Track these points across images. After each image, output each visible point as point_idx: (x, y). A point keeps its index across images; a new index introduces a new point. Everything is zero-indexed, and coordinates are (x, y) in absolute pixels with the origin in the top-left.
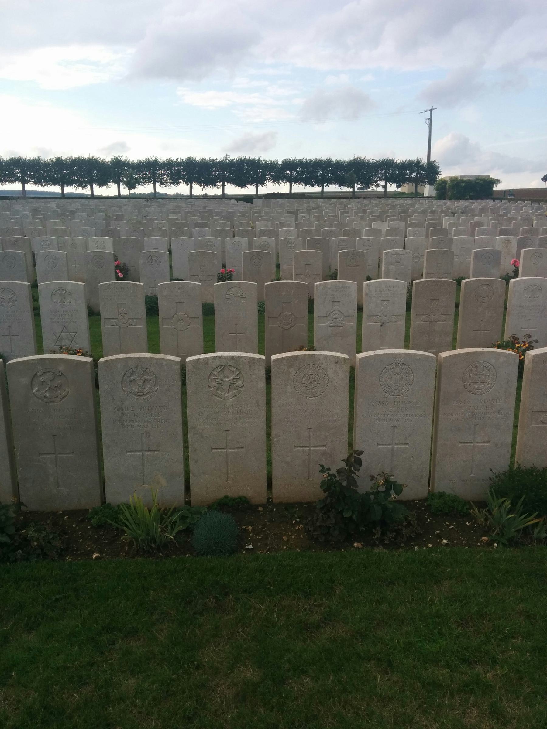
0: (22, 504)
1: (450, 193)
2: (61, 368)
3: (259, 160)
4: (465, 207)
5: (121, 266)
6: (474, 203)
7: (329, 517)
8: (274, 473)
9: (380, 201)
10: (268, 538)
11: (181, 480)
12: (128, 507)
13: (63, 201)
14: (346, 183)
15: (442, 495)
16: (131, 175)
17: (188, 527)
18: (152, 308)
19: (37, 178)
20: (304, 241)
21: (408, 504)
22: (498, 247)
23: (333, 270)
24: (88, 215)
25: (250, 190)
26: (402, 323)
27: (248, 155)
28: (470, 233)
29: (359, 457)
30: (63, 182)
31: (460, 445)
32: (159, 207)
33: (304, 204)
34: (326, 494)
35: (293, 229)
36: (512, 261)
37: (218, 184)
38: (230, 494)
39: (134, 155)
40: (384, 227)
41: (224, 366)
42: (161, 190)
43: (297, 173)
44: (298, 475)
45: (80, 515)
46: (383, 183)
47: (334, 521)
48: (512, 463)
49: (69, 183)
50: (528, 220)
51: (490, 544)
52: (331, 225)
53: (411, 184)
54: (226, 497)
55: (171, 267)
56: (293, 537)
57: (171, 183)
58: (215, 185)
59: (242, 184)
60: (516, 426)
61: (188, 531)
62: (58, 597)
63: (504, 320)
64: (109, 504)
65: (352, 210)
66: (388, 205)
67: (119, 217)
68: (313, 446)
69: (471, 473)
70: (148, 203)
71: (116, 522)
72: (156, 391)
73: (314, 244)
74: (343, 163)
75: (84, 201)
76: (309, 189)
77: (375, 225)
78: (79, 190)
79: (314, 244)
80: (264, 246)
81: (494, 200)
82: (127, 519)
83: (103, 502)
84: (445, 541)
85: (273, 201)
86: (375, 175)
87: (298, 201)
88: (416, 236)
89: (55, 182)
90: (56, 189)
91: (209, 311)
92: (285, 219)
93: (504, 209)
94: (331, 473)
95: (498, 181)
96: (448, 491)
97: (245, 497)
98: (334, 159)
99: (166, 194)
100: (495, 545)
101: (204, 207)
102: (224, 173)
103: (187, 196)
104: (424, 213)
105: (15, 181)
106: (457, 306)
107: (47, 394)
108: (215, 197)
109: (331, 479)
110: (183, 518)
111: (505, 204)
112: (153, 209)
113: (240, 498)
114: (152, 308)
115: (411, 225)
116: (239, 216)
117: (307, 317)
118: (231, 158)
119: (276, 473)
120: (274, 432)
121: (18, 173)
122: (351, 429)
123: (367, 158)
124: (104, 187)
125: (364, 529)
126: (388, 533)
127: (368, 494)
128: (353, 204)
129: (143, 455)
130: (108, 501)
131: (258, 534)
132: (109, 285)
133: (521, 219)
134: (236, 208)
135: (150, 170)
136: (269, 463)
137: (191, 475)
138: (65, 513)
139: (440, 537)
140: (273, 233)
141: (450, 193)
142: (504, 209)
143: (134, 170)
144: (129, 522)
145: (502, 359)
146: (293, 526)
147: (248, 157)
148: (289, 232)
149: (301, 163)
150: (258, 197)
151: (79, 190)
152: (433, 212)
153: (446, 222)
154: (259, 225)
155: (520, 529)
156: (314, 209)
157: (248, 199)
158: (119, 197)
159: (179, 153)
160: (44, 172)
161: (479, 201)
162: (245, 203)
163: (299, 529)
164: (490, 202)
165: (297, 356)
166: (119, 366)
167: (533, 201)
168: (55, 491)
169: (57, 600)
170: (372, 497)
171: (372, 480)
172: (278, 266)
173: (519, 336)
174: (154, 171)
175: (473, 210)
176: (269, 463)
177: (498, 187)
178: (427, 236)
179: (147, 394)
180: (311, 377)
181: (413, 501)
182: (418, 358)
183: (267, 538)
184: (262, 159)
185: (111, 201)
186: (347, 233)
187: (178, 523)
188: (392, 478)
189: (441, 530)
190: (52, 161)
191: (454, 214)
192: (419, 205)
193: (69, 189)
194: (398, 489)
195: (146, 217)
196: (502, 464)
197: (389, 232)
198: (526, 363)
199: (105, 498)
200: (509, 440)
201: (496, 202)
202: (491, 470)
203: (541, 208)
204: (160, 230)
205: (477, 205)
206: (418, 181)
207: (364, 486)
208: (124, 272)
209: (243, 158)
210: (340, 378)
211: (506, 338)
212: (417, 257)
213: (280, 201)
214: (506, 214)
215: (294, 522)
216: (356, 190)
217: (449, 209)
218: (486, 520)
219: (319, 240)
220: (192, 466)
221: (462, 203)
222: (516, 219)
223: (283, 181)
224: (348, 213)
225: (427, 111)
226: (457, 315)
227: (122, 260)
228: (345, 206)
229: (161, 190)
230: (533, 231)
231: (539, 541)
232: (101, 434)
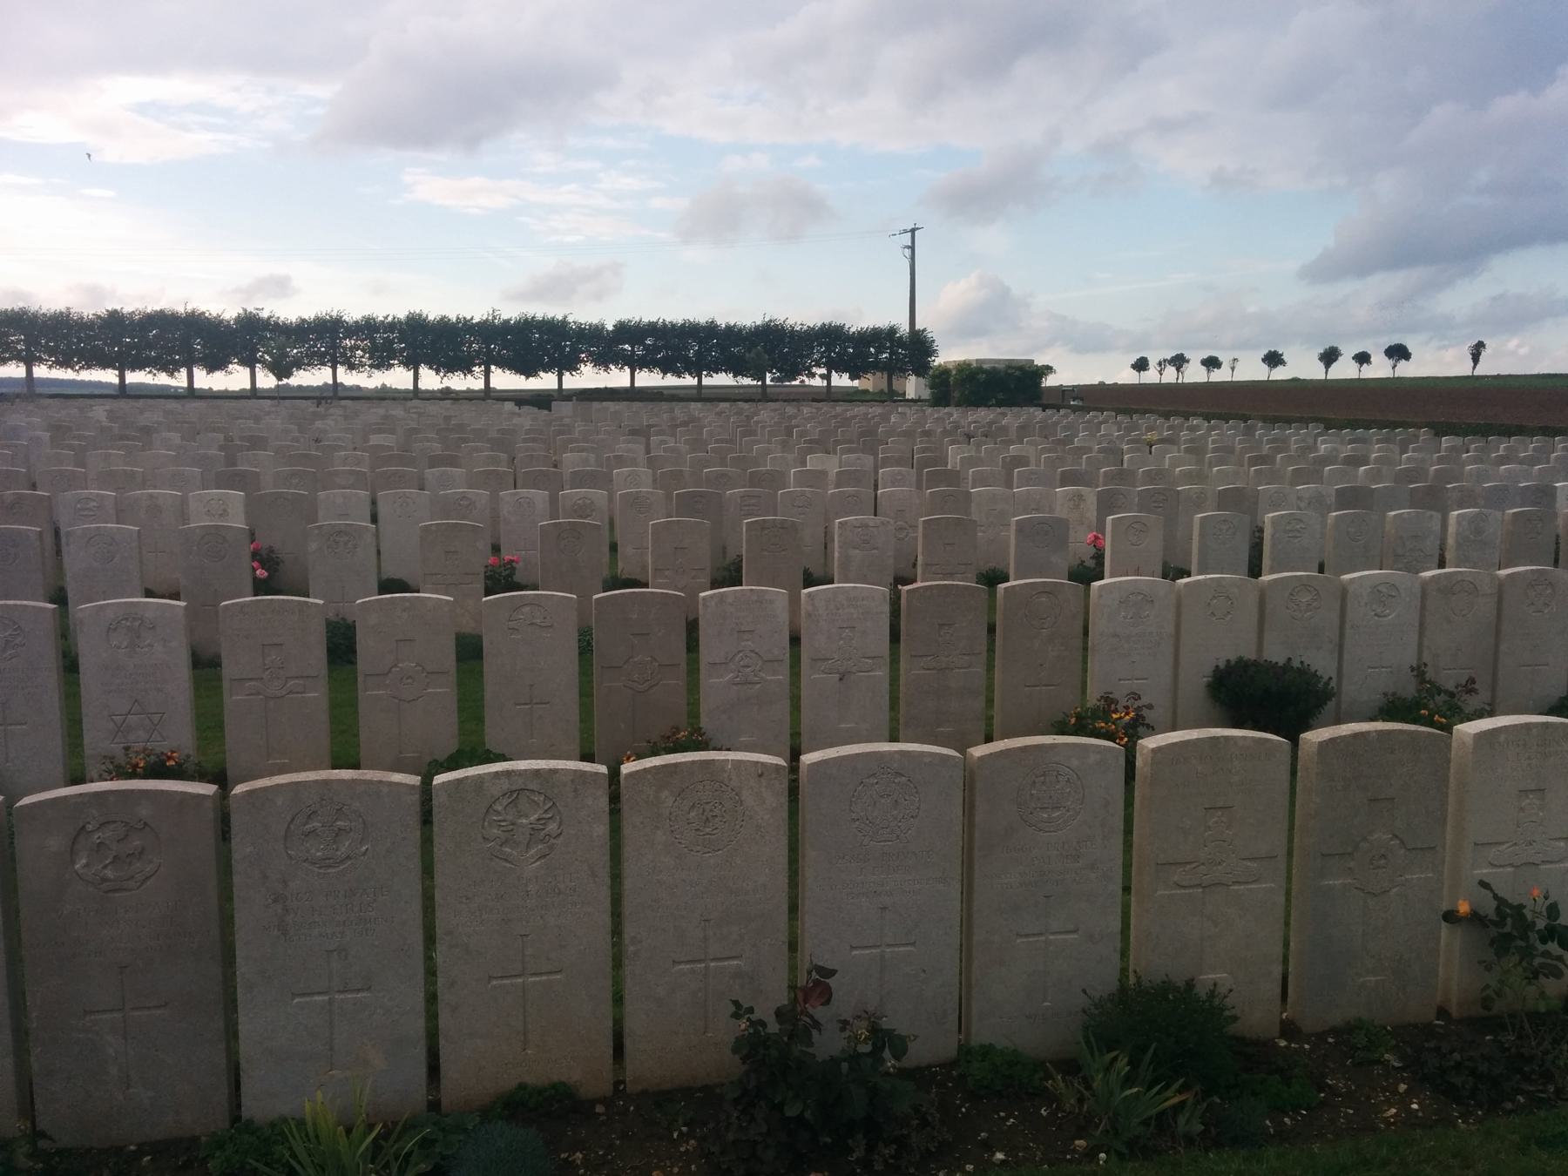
0: (43, 1135)
1: (956, 394)
2: (144, 811)
3: (564, 322)
4: (990, 424)
5: (264, 553)
6: (1005, 415)
9: (819, 409)
11: (420, 1052)
12: (301, 1123)
13: (123, 404)
14: (748, 370)
15: (986, 1051)
16: (282, 348)
18: (341, 645)
19: (63, 353)
20: (669, 497)
21: (920, 1076)
22: (1061, 512)
23: (731, 556)
24: (183, 438)
25: (546, 381)
26: (882, 673)
27: (541, 310)
28: (1010, 487)
30: (123, 363)
32: (346, 417)
33: (663, 412)
34: (745, 1068)
35: (644, 471)
36: (1090, 536)
37: (476, 369)
38: (530, 1080)
39: (289, 310)
40: (832, 465)
41: (519, 790)
42: (347, 378)
43: (646, 348)
44: (682, 1027)
46: (823, 371)
48: (1124, 971)
49: (138, 365)
50: (1114, 454)
51: (1090, 1154)
52: (723, 463)
53: (879, 374)
55: (379, 552)
57: (371, 366)
58: (471, 372)
59: (528, 371)
60: (1127, 889)
63: (1085, 662)
64: (250, 1122)
65: (763, 427)
66: (835, 417)
67: (256, 442)
68: (714, 960)
70: (321, 409)
71: (266, 1164)
72: (365, 854)
73: (689, 504)
74: (740, 330)
75: (172, 405)
76: (671, 380)
77: (814, 462)
78: (162, 379)
79: (689, 504)
80: (584, 509)
81: (1045, 408)
82: (294, 1156)
83: (236, 1119)
84: (1000, 1156)
85: (596, 405)
86: (808, 356)
87: (650, 405)
88: (895, 487)
89: (105, 364)
90: (109, 376)
91: (470, 651)
92: (623, 447)
93: (1065, 428)
94: (754, 1017)
95: (1048, 369)
98: (722, 322)
99: (358, 387)
100: (1103, 1155)
101: (447, 419)
102: (488, 347)
103: (407, 391)
104: (909, 434)
105: (10, 359)
106: (991, 629)
107: (109, 873)
108: (469, 396)
109: (757, 1032)
110: (426, 1143)
111: (1066, 416)
112: (332, 423)
113: (554, 1086)
114: (341, 645)
115: (886, 462)
116: (525, 441)
117: (684, 666)
118: (505, 317)
119: (635, 1024)
120: (629, 930)
121: (18, 342)
122: (793, 909)
123: (790, 322)
124: (218, 375)
125: (829, 1140)
127: (834, 1061)
128: (766, 414)
129: (331, 1002)
130: (246, 1113)
132: (243, 605)
133: (1100, 451)
134: (516, 420)
135: (326, 338)
136: (618, 1000)
137: (442, 1042)
138: (141, 1152)
139: (989, 1147)
140: (600, 479)
141: (956, 394)
142: (1065, 428)
143: (288, 338)
144: (299, 1163)
145: (1093, 758)
147: (539, 316)
148: (634, 479)
149: (653, 329)
150: (562, 395)
151: (162, 379)
152: (927, 433)
153: (955, 455)
154: (571, 461)
155: (1150, 1118)
156: (685, 424)
157: (541, 400)
158: (254, 393)
159: (392, 307)
160: (80, 340)
161: (1015, 409)
162: (536, 410)
164: (1038, 414)
165: (676, 765)
166: (279, 803)
167: (1119, 411)
170: (845, 1066)
171: (843, 1029)
172: (614, 548)
173: (1115, 696)
174: (333, 340)
175: (1004, 429)
176: (618, 1000)
177: (1050, 381)
178: (919, 486)
179: (342, 862)
180: (708, 807)
181: (929, 1067)
182: (927, 760)
184: (570, 319)
185: (234, 403)
186: (755, 480)
187: (413, 1159)
188: (885, 1024)
190: (99, 317)
191: (969, 436)
192: (901, 418)
193: (134, 377)
194: (899, 1045)
195: (317, 441)
196: (1104, 980)
197: (844, 478)
198: (1139, 763)
199: (239, 1106)
200: (1117, 925)
201: (1049, 412)
202: (1084, 991)
203: (1135, 427)
204: (351, 472)
205: (1011, 418)
206: (893, 369)
207: (828, 1044)
208: (273, 575)
209: (530, 316)
210: (768, 805)
211: (1093, 698)
212: (901, 529)
213: (612, 406)
214: (1068, 440)
216: (768, 382)
217: (957, 427)
218: (1081, 1101)
219: (701, 495)
220: (445, 1020)
221: (983, 415)
222: (1090, 450)
223: (616, 364)
224: (753, 433)
225: (905, 231)
226: (991, 650)
227: (264, 542)
228: (748, 418)
229: (347, 378)
230: (1123, 476)
231: (1189, 1141)
232: (234, 956)
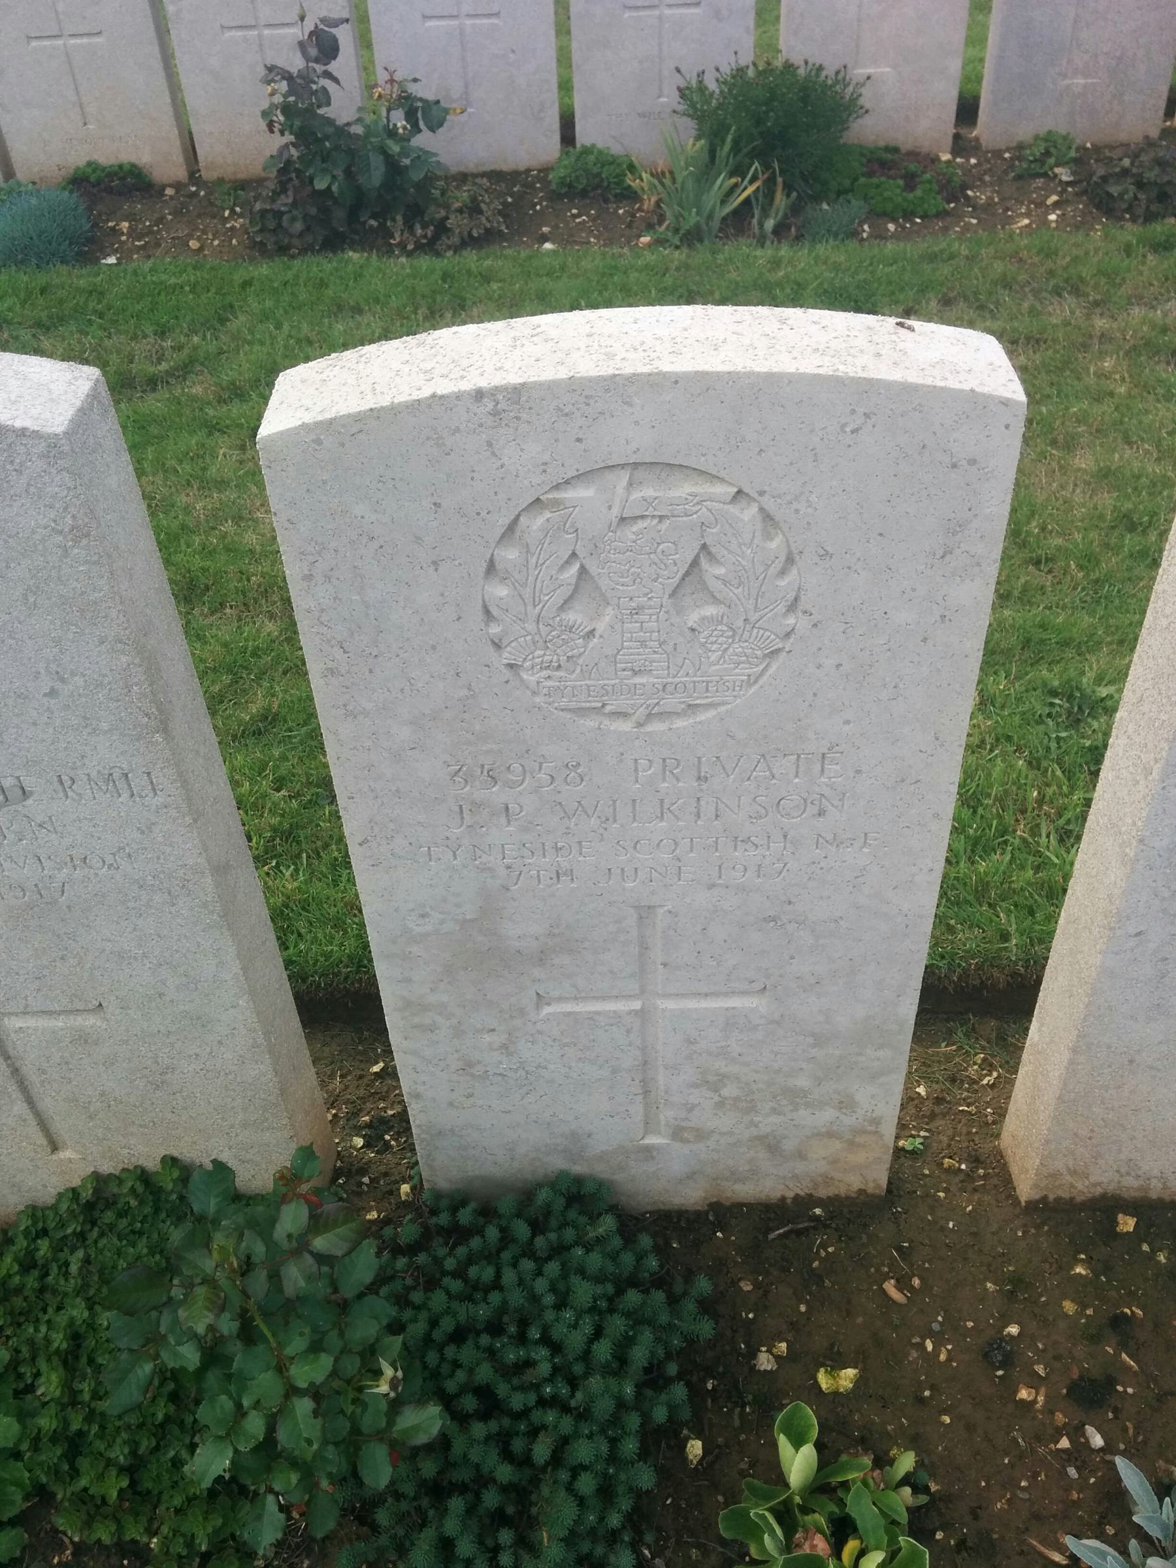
10: (160, 245)
29: (333, 31)
31: (627, 15)
47: (290, 200)
56: (216, 242)
97: (133, 165)
119: (194, 100)
129: (260, 36)
139: (544, 239)
146: (226, 220)
163: (233, 228)
181: (528, 171)
183: (158, 245)
215: (227, 213)
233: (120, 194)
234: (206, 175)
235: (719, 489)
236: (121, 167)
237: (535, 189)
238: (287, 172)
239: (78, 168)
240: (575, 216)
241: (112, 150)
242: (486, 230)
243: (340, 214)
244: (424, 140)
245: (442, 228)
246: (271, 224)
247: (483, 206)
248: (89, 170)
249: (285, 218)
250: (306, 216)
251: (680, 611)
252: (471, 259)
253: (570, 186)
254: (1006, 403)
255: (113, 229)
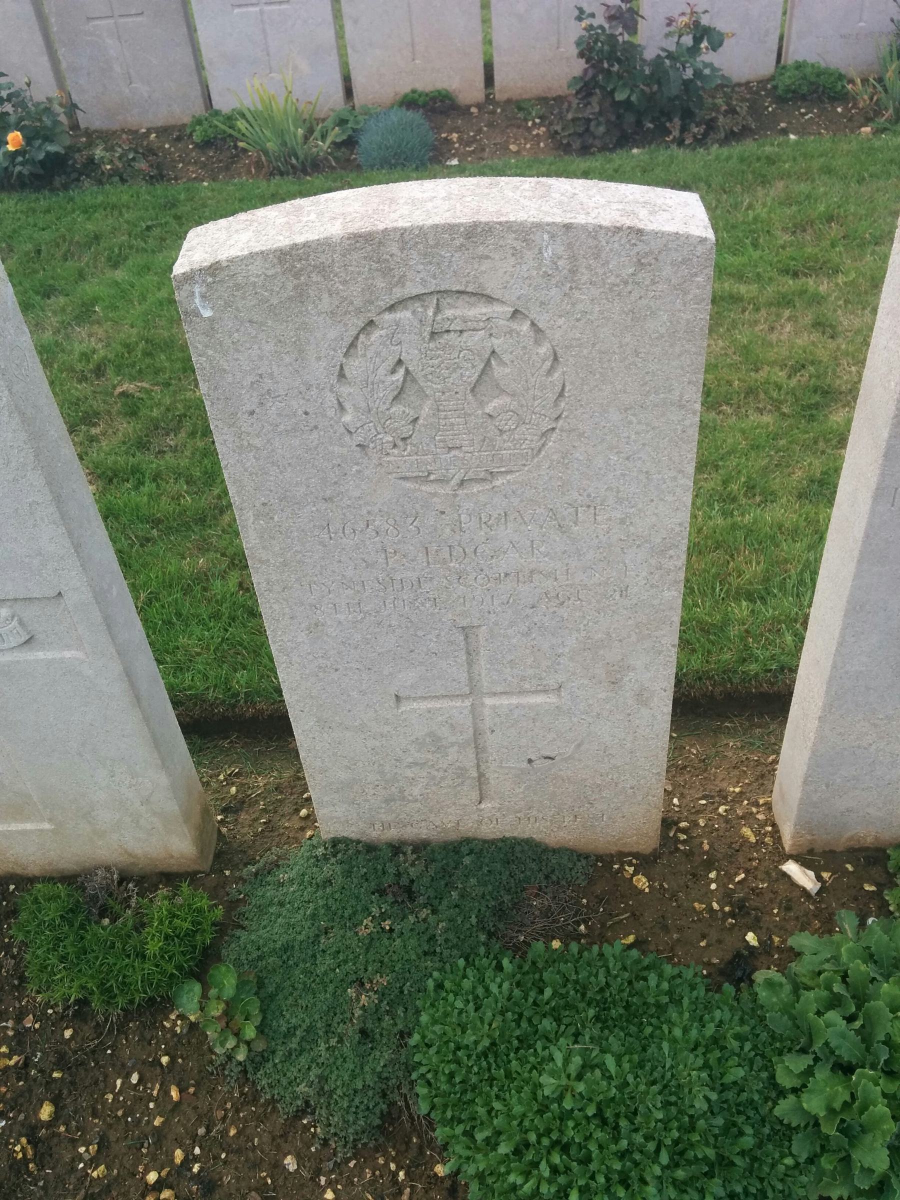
7: (589, 103)
8: (497, 61)
17: (350, 137)
38: (420, 87)
45: (175, 133)
47: (597, 110)
54: (414, 91)
56: (528, 146)
61: (350, 143)
62: (149, 223)
69: (860, 21)
96: (811, 59)
119: (502, 35)
125: (651, 126)
126: (693, 125)
129: (262, 12)
130: (217, 105)
131: (468, 144)
137: (349, 51)
138: (149, 131)
139: (785, 132)
146: (529, 130)
163: (538, 135)
168: (127, 91)
169: (149, 228)
181: (748, 83)
183: (483, 150)
189: (789, 123)
215: (530, 124)
233: (441, 113)
234: (500, 96)
235: (498, 308)
236: (438, 91)
237: (761, 96)
238: (586, 88)
239: (406, 96)
240: (804, 115)
241: (429, 80)
242: (743, 126)
243: (630, 118)
244: (707, 56)
245: (711, 126)
246: (581, 130)
247: (738, 109)
248: (416, 96)
249: (593, 123)
250: (608, 121)
251: (482, 404)
252: (748, 146)
253: (794, 92)
254: (703, 240)
255: (446, 139)
